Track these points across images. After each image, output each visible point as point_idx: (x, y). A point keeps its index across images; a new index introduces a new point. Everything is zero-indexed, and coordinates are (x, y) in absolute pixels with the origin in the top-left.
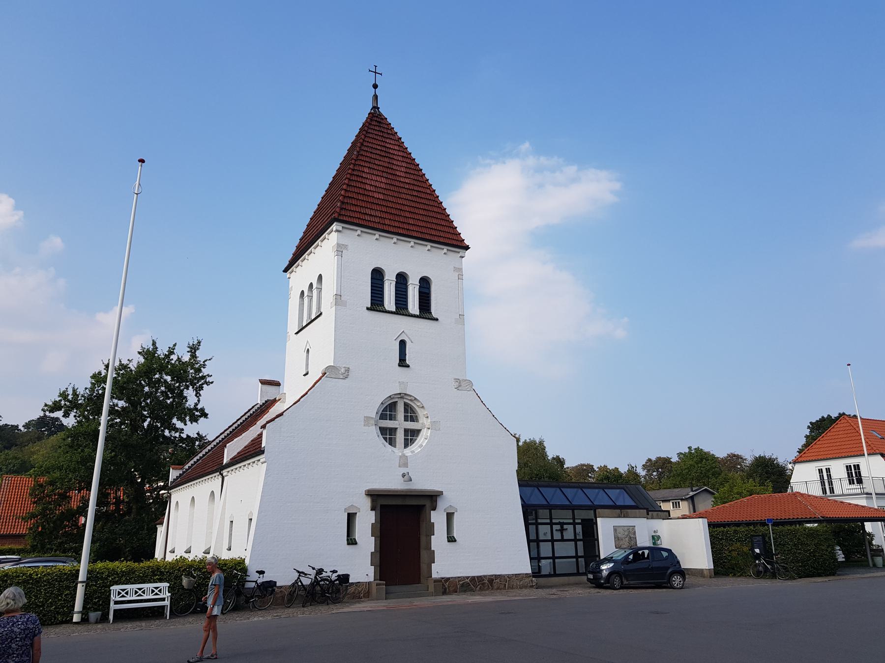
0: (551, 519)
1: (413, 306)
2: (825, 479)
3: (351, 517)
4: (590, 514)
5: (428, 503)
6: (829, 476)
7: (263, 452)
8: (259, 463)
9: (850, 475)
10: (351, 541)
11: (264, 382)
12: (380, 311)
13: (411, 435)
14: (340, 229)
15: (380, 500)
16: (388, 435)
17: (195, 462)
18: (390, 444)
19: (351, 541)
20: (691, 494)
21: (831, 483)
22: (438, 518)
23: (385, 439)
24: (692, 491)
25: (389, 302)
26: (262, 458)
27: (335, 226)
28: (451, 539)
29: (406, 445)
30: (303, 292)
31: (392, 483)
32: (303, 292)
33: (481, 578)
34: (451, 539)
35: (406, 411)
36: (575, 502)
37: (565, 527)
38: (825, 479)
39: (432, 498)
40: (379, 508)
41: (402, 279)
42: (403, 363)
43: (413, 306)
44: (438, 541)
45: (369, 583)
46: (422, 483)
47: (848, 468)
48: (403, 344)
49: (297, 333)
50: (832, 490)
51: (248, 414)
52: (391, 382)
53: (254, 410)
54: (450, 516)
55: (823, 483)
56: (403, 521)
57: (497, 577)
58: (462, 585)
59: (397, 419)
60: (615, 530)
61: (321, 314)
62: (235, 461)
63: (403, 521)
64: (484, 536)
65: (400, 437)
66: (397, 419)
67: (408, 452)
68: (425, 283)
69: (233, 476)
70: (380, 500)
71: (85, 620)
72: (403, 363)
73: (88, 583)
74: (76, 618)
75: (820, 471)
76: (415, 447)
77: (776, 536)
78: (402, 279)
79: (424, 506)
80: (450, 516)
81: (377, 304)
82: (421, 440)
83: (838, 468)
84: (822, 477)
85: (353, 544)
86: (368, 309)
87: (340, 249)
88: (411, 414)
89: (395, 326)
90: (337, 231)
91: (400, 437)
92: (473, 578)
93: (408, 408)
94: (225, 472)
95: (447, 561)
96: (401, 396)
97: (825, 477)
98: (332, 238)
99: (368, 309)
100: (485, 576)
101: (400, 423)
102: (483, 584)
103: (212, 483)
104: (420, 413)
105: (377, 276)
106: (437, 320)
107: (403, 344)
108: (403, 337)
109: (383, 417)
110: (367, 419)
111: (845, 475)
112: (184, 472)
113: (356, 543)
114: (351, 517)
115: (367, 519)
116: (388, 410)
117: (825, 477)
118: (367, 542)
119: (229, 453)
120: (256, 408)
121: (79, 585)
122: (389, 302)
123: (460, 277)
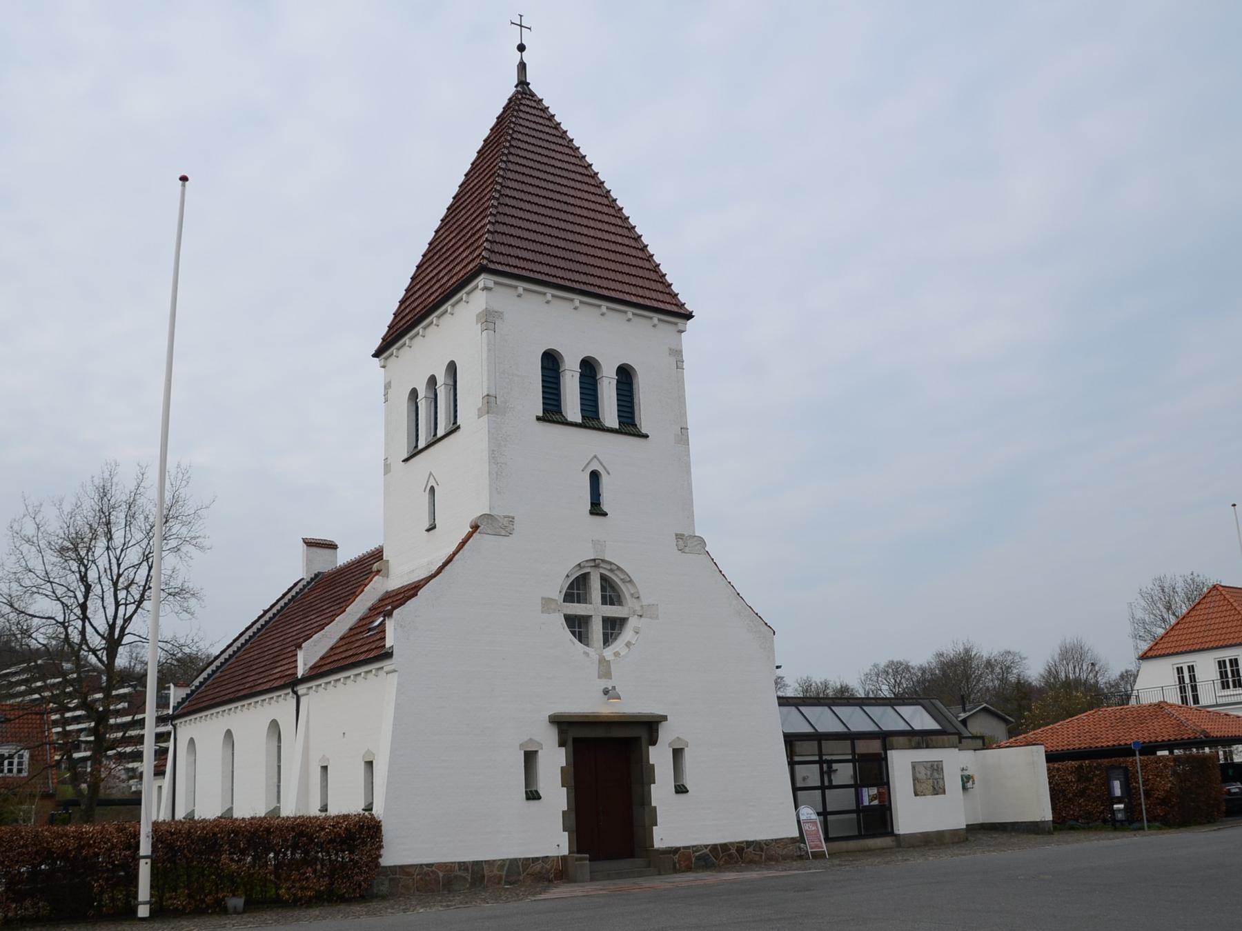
0: (820, 755)
1: (609, 415)
2: (1188, 684)
3: (530, 757)
4: (874, 747)
5: (643, 734)
6: (1193, 678)
7: (388, 655)
8: (381, 673)
9: (1223, 675)
10: (533, 795)
11: (310, 544)
12: (594, 428)
13: (613, 627)
14: (491, 284)
15: (570, 729)
16: (578, 625)
17: (210, 676)
18: (580, 641)
19: (533, 795)
20: (963, 715)
21: (1194, 688)
22: (659, 756)
23: (573, 633)
24: (964, 711)
25: (572, 407)
26: (387, 665)
27: (483, 280)
28: (681, 789)
29: (607, 641)
30: (414, 393)
31: (586, 701)
32: (414, 393)
33: (725, 847)
34: (681, 789)
35: (603, 589)
36: (821, 729)
37: (835, 766)
38: (1188, 684)
39: (649, 727)
40: (570, 742)
41: (589, 368)
42: (596, 509)
43: (609, 415)
44: (661, 792)
45: (564, 858)
46: (632, 704)
47: (1221, 664)
48: (595, 477)
49: (406, 460)
50: (1196, 700)
51: (289, 596)
52: (576, 542)
53: (297, 589)
54: (678, 754)
55: (1182, 690)
56: (608, 764)
57: (749, 843)
58: (698, 858)
59: (594, 601)
60: (914, 768)
61: (458, 427)
62: (321, 671)
63: (608, 764)
64: (726, 787)
65: (597, 629)
66: (594, 601)
67: (608, 653)
68: (625, 375)
69: (317, 698)
70: (570, 729)
71: (159, 912)
72: (596, 509)
73: (155, 860)
74: (143, 911)
75: (1180, 670)
76: (618, 645)
77: (1128, 776)
78: (589, 368)
79: (638, 739)
80: (678, 754)
81: (552, 411)
82: (627, 634)
83: (1206, 666)
84: (1181, 680)
85: (534, 799)
86: (538, 419)
87: (489, 319)
88: (611, 594)
89: (577, 448)
90: (486, 288)
91: (597, 629)
92: (714, 848)
93: (606, 582)
94: (301, 689)
95: (675, 824)
96: (595, 563)
97: (1187, 680)
98: (478, 298)
99: (538, 419)
100: (732, 844)
101: (595, 609)
102: (730, 855)
103: (279, 707)
104: (625, 590)
105: (551, 361)
106: (646, 436)
107: (595, 477)
108: (595, 466)
109: (569, 597)
110: (547, 603)
111: (1215, 675)
112: (193, 692)
113: (539, 798)
114: (530, 757)
115: (553, 760)
116: (577, 589)
117: (1187, 680)
118: (556, 797)
119: (304, 661)
120: (300, 586)
121: (142, 862)
122: (572, 407)
123: (679, 364)
